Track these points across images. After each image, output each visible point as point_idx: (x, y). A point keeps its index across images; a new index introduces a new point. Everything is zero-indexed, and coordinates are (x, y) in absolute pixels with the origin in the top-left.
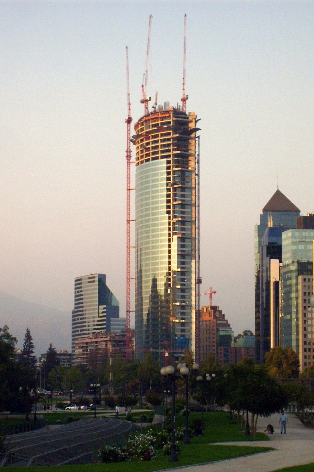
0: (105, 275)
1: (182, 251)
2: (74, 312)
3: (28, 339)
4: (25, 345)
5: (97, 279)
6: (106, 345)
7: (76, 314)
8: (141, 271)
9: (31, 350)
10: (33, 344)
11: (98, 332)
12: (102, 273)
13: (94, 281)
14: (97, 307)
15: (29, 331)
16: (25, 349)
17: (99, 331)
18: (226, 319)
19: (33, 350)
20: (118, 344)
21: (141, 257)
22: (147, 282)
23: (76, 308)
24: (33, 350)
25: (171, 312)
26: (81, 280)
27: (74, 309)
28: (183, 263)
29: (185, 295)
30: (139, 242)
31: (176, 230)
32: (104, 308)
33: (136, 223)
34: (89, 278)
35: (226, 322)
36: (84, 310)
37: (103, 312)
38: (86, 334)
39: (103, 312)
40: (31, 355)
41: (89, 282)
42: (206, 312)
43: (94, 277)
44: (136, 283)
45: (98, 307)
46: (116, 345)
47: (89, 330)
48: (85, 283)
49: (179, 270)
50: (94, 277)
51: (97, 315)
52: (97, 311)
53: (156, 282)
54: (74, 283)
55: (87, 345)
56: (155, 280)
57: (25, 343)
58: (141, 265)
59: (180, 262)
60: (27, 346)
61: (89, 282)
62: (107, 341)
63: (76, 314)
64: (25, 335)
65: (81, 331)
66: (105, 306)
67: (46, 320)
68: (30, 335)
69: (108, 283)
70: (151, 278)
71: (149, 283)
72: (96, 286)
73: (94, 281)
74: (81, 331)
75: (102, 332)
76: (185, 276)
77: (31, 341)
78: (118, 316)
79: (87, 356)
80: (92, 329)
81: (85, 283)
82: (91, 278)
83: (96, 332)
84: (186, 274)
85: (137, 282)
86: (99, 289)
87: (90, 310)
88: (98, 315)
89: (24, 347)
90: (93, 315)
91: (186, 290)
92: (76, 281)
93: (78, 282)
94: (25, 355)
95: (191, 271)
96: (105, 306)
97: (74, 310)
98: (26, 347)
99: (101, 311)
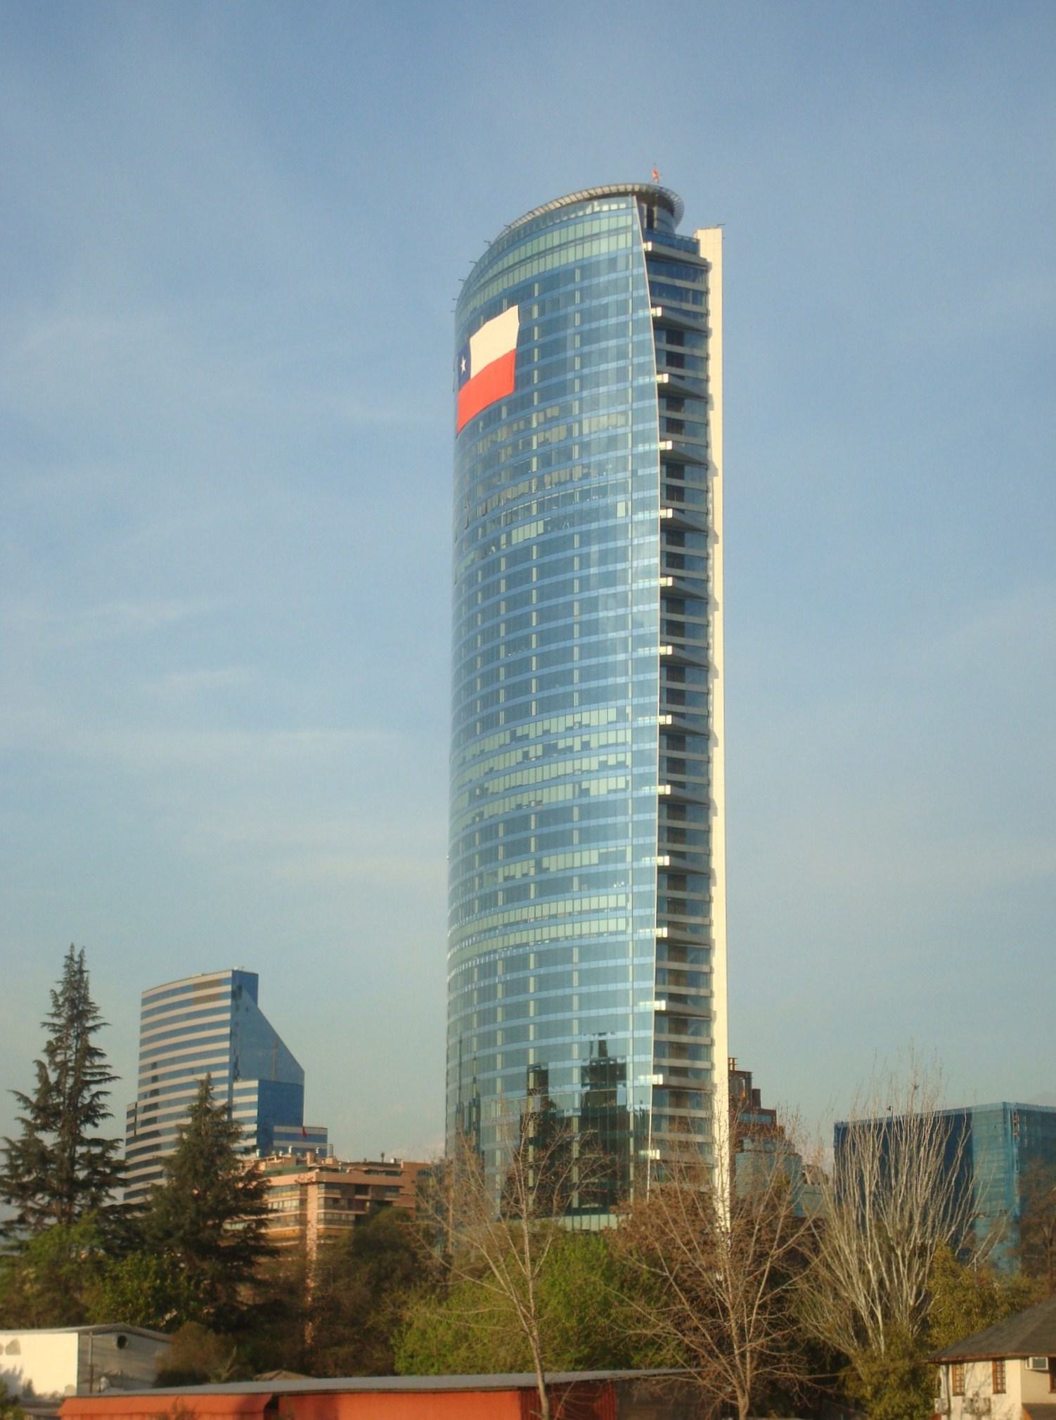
3: (71, 1020)
4: (45, 1059)
6: (303, 1202)
9: (86, 1097)
10: (102, 1055)
15: (81, 972)
16: (47, 1088)
18: (766, 1104)
19: (102, 1100)
20: (350, 1201)
24: (102, 1100)
35: (766, 1119)
40: (88, 1132)
46: (343, 1203)
57: (51, 1050)
60: (63, 1067)
62: (303, 1186)
64: (55, 996)
68: (84, 999)
69: (268, 1003)
77: (94, 1040)
78: (298, 1120)
89: (43, 1078)
92: (145, 1001)
94: (44, 1127)
98: (53, 1077)
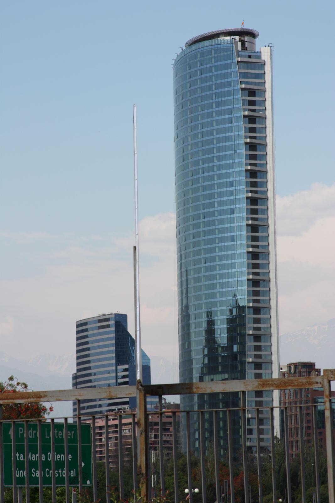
0: (127, 315)
1: (254, 274)
2: (75, 377)
5: (112, 322)
7: (78, 380)
8: (165, 482)
11: (119, 409)
12: (121, 313)
13: (108, 326)
14: (114, 368)
17: (119, 407)
21: (187, 276)
22: (198, 316)
23: (78, 370)
25: (239, 355)
26: (85, 324)
27: (76, 372)
28: (255, 239)
29: (260, 346)
30: (183, 261)
31: (248, 336)
32: (125, 370)
33: (196, 106)
34: (100, 321)
36: (93, 374)
37: (124, 377)
38: (95, 406)
39: (124, 377)
41: (100, 328)
42: (295, 372)
43: (108, 320)
44: (181, 345)
45: (116, 368)
47: (100, 406)
48: (93, 329)
49: (251, 305)
50: (108, 320)
51: (115, 381)
52: (114, 374)
53: (214, 325)
54: (74, 330)
55: (100, 431)
56: (211, 323)
58: (187, 288)
59: (249, 184)
61: (100, 328)
63: (78, 380)
65: (88, 407)
66: (126, 366)
67: (43, 364)
70: (204, 310)
71: (202, 309)
72: (111, 333)
73: (108, 326)
74: (88, 407)
75: (125, 409)
76: (255, 96)
79: (101, 448)
80: (107, 405)
81: (93, 329)
82: (103, 320)
83: (115, 410)
84: (262, 312)
85: (182, 353)
86: (117, 339)
87: (100, 373)
88: (117, 381)
90: (108, 382)
91: (258, 174)
92: (78, 326)
93: (82, 327)
95: (270, 278)
96: (126, 366)
97: (76, 374)
99: (120, 374)
